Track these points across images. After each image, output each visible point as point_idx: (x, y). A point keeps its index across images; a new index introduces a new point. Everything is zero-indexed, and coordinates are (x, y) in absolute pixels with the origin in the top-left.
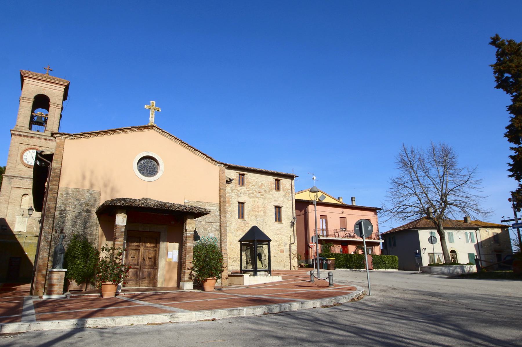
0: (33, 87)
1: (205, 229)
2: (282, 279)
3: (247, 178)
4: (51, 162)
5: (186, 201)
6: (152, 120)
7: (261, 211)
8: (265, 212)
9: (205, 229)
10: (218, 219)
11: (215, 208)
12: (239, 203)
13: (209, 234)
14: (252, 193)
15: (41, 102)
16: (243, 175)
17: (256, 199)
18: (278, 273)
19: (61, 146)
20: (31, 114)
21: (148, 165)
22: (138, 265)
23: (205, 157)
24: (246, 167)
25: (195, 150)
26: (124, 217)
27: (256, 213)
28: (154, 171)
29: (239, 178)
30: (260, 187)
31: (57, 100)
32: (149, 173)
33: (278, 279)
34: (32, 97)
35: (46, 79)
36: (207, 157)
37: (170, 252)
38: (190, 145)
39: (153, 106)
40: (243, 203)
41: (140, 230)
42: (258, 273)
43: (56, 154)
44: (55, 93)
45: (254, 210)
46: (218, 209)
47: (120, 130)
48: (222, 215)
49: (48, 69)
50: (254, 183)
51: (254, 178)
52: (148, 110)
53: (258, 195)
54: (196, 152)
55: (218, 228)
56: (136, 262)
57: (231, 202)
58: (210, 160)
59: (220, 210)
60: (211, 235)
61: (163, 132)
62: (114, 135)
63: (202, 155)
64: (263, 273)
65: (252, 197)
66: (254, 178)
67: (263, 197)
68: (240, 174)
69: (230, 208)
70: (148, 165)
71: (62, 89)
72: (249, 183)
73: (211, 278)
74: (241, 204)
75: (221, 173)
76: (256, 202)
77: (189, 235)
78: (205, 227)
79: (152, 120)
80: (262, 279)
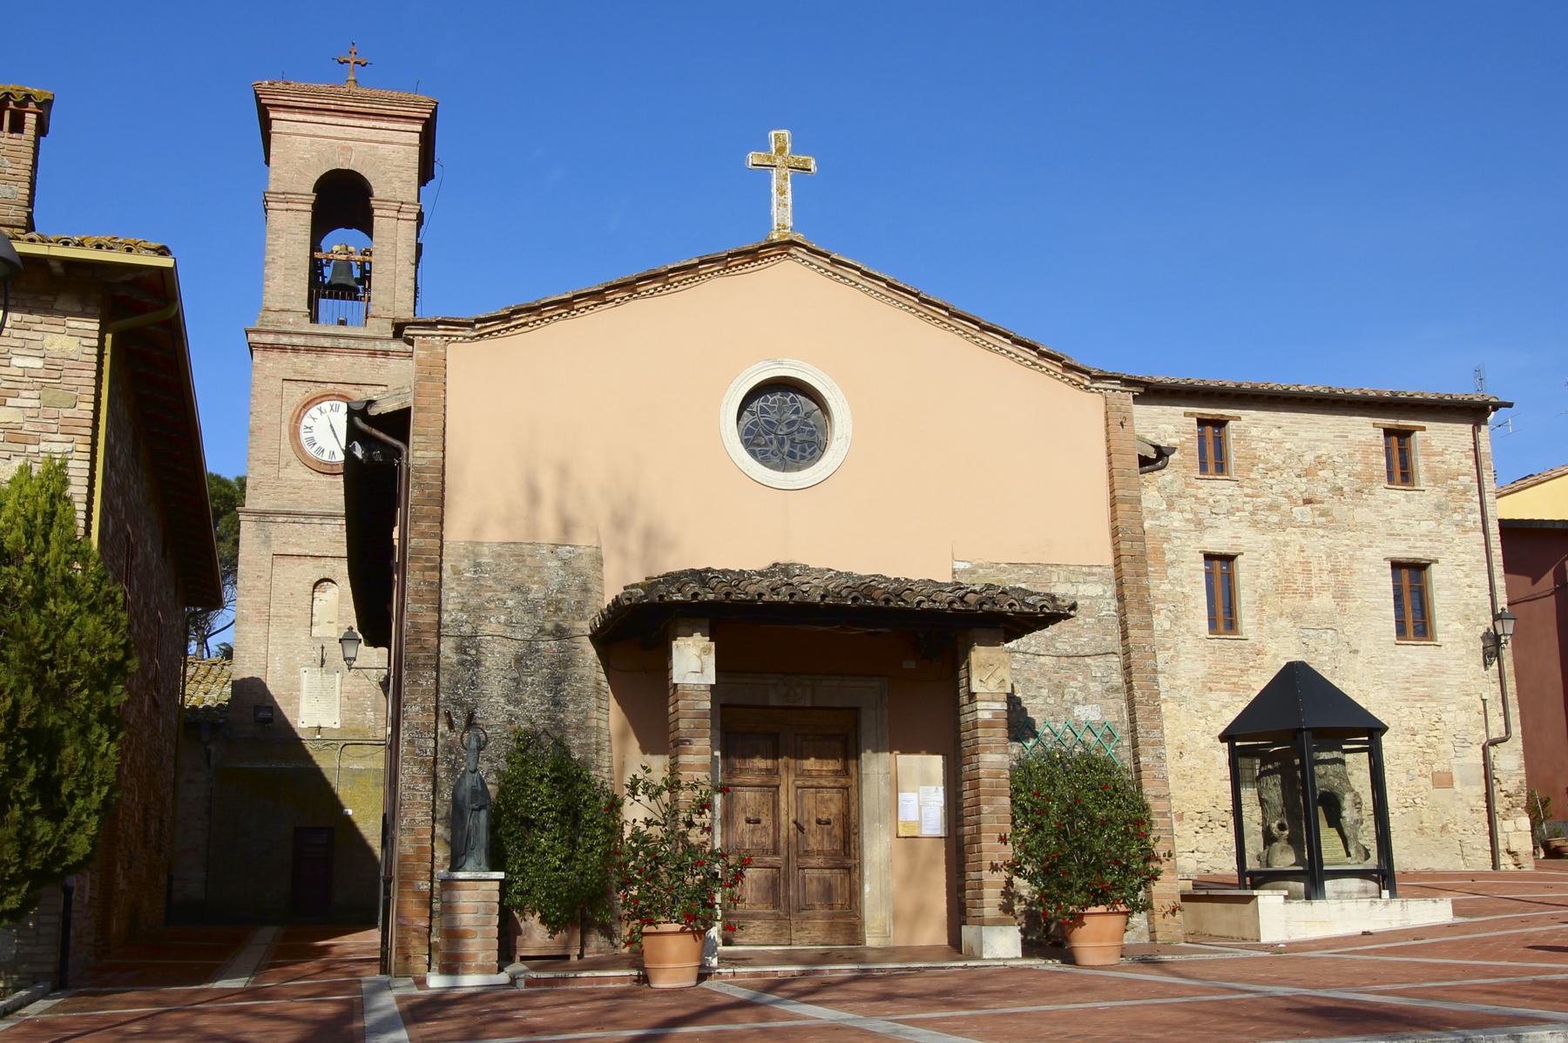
0: (306, 148)
1: (1058, 689)
2: (1457, 912)
3: (1242, 436)
5: (959, 566)
7: (1323, 588)
8: (1342, 594)
9: (1058, 689)
10: (1113, 641)
11: (1097, 590)
12: (1209, 557)
14: (1273, 507)
15: (342, 200)
16: (1220, 423)
17: (1293, 536)
18: (1430, 885)
19: (435, 374)
21: (784, 420)
22: (776, 852)
23: (1032, 356)
24: (1230, 384)
25: (984, 328)
27: (1298, 601)
28: (811, 444)
29: (1201, 438)
30: (1308, 473)
31: (397, 184)
32: (792, 455)
33: (1436, 912)
34: (307, 186)
35: (350, 105)
36: (1043, 355)
37: (908, 794)
39: (781, 150)
40: (1229, 559)
41: (773, 701)
42: (1328, 884)
43: (420, 410)
44: (384, 155)
45: (1283, 587)
46: (1111, 590)
47: (654, 277)
48: (1133, 618)
49: (352, 58)
50: (1277, 460)
53: (1303, 513)
54: (988, 337)
55: (1117, 679)
57: (1169, 557)
58: (1055, 368)
60: (1088, 713)
61: (835, 262)
63: (1015, 349)
64: (1354, 884)
65: (1269, 528)
67: (1330, 522)
68: (1202, 422)
69: (1166, 587)
70: (784, 420)
71: (410, 135)
72: (1253, 460)
73: (1102, 909)
74: (1220, 563)
75: (1115, 423)
78: (1056, 678)
79: (782, 217)
80: (1346, 913)
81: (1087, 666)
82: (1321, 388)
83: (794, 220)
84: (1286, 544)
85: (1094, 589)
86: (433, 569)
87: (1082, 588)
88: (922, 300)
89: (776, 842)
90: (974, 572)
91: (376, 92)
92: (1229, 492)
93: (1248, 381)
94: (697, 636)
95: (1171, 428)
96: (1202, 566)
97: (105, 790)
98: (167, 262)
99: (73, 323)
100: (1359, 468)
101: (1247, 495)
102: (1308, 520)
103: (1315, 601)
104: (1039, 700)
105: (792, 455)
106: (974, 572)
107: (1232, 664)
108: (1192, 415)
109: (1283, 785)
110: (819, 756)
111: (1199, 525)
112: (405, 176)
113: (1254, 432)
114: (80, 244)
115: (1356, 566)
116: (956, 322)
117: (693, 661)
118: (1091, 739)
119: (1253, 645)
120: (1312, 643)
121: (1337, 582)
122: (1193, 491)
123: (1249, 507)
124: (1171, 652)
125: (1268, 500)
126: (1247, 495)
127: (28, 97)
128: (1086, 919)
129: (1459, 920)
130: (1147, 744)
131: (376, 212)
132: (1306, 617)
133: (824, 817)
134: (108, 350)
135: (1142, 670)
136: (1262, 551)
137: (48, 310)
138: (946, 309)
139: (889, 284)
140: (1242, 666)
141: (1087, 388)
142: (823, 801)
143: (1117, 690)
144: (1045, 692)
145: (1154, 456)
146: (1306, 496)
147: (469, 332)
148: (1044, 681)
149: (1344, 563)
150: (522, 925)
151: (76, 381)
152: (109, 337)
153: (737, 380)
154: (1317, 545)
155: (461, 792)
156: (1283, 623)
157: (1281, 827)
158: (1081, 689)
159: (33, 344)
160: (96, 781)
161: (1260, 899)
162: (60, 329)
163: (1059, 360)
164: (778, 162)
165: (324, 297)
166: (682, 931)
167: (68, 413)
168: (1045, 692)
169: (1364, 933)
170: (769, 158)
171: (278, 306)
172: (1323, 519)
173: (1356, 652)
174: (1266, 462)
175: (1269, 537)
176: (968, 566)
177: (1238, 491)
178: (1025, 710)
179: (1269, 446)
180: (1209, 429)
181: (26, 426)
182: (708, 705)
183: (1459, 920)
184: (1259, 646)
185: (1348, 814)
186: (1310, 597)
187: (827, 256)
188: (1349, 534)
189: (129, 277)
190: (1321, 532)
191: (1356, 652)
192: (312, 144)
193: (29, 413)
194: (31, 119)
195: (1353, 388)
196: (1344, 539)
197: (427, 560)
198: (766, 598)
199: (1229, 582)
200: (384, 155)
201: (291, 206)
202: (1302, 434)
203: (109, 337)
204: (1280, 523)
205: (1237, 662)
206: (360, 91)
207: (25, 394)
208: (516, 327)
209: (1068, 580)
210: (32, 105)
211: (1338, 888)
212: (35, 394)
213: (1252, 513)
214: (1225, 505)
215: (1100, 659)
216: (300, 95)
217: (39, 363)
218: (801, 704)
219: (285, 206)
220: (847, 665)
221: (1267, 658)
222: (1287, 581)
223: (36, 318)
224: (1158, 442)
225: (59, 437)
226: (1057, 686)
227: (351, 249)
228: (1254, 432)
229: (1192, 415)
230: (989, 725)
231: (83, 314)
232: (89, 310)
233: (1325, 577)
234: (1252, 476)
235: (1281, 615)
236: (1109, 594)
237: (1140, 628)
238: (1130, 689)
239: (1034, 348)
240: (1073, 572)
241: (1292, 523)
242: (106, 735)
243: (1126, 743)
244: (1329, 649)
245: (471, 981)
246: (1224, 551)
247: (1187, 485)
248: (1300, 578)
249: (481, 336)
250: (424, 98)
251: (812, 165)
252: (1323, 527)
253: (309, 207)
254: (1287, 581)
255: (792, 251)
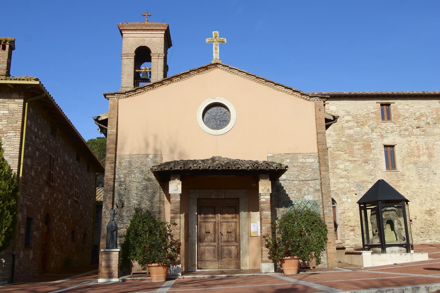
0: (132, 41)
1: (300, 191)
2: (430, 256)
3: (395, 108)
4: (107, 126)
5: (269, 155)
6: (216, 56)
7: (424, 154)
8: (430, 156)
9: (300, 191)
10: (317, 176)
11: (313, 160)
12: (385, 146)
13: (306, 197)
14: (406, 130)
15: (143, 55)
16: (388, 105)
17: (413, 138)
18: (422, 248)
19: (116, 108)
20: (135, 71)
21: (216, 114)
22: (215, 241)
23: (291, 91)
24: (390, 93)
25: (276, 84)
26: (178, 184)
27: (416, 159)
28: (225, 121)
29: (382, 110)
30: (418, 118)
31: (158, 49)
32: (220, 125)
33: (423, 257)
34: (133, 52)
35: (144, 28)
36: (294, 91)
37: (255, 225)
38: (268, 79)
39: (216, 37)
40: (393, 146)
41: (213, 197)
42: (388, 249)
43: (111, 118)
44: (155, 41)
45: (411, 154)
46: (317, 160)
47: (177, 76)
48: (323, 168)
49: (146, 14)
50: (407, 115)
51: (407, 107)
52: (211, 43)
53: (415, 131)
54: (278, 87)
55: (318, 187)
56: (212, 238)
57: (372, 147)
58: (298, 95)
59: (319, 162)
60: (309, 198)
61: (230, 68)
62: (172, 84)
63: (286, 90)
64: (397, 248)
65: (405, 136)
66: (407, 107)
67: (425, 133)
68: (382, 105)
69: (371, 156)
70: (216, 114)
71: (161, 35)
72: (399, 116)
73: (289, 257)
74: (389, 149)
75: (318, 110)
76: (414, 142)
77: (264, 200)
78: (299, 187)
79: (216, 56)
80: (393, 257)
81: (309, 183)
82: (420, 92)
83: (219, 57)
84: (411, 141)
85: (311, 160)
86: (112, 163)
87: (307, 160)
88: (257, 77)
89: (215, 239)
90: (273, 157)
91: (159, 23)
92: (392, 126)
93: (395, 91)
94: (176, 180)
95: (372, 107)
96: (383, 149)
97: (6, 228)
98: (38, 83)
99: (16, 101)
100: (435, 116)
101: (397, 127)
102: (418, 133)
103: (422, 158)
104: (294, 194)
105: (220, 125)
106: (273, 157)
107: (394, 179)
108: (379, 103)
109: (377, 218)
110: (228, 214)
111: (382, 136)
112: (160, 46)
113: (399, 107)
114: (23, 80)
115: (435, 147)
116: (267, 83)
117: (175, 187)
118: (309, 206)
119: (401, 173)
120: (421, 172)
121: (429, 152)
122: (380, 126)
123: (398, 130)
124: (374, 176)
125: (405, 128)
126: (397, 127)
127: (6, 41)
128: (285, 261)
129: (430, 259)
130: (326, 206)
131: (152, 57)
132: (418, 163)
133: (229, 231)
134: (26, 107)
135: (325, 184)
136: (403, 143)
137: (10, 97)
138: (264, 80)
139: (246, 74)
140: (397, 180)
141: (309, 100)
142: (229, 226)
143: (318, 190)
144: (295, 192)
145: (333, 119)
146: (417, 126)
147: (124, 96)
148: (295, 189)
149: (431, 146)
150: (133, 264)
151: (17, 116)
152: (27, 104)
153: (202, 104)
154: (421, 141)
155: (402, 219)
156: (411, 166)
157: (376, 231)
158: (307, 191)
159: (6, 107)
160: (4, 225)
161: (363, 254)
162: (13, 102)
163: (299, 92)
164: (215, 41)
165: (140, 82)
166: (159, 266)
167: (14, 125)
168: (295, 192)
169: (395, 264)
170: (212, 40)
171: (125, 86)
172: (423, 133)
173: (436, 174)
174: (404, 116)
175: (405, 139)
176: (272, 155)
177: (394, 125)
178: (289, 198)
179: (404, 111)
180: (385, 107)
181: (4, 129)
182: (179, 199)
183: (430, 259)
184: (403, 173)
185: (396, 226)
186: (420, 157)
187: (228, 67)
188: (432, 137)
189: (30, 87)
190: (423, 137)
191: (436, 174)
192: (134, 39)
193: (4, 125)
194: (7, 46)
195: (431, 92)
196: (430, 139)
197: (111, 160)
198: (192, 168)
199: (393, 153)
200: (155, 41)
201: (128, 57)
202: (415, 107)
203: (27, 104)
204: (409, 135)
205: (396, 178)
206: (149, 23)
207: (3, 120)
208: (138, 93)
209: (303, 158)
210: (8, 43)
211: (391, 250)
212: (6, 120)
213: (399, 132)
214: (391, 130)
215: (313, 181)
216: (130, 26)
217: (7, 112)
218: (221, 198)
219: (127, 57)
220: (221, 187)
221: (406, 177)
222: (412, 152)
223: (7, 100)
224: (334, 114)
225: (12, 131)
226: (299, 190)
227: (147, 68)
228: (399, 107)
229: (379, 103)
230: (264, 203)
231: (19, 98)
232: (21, 97)
233: (424, 151)
234: (399, 120)
235: (410, 163)
236: (316, 161)
237: (325, 171)
238: (322, 190)
239: (291, 89)
240: (305, 155)
241: (413, 134)
242: (9, 213)
243: (321, 206)
244: (427, 173)
245: (115, 280)
246: (390, 144)
247: (378, 124)
248: (416, 152)
249: (128, 96)
250: (165, 24)
251: (225, 41)
252: (424, 135)
253: (134, 57)
254: (412, 152)
255: (218, 66)
